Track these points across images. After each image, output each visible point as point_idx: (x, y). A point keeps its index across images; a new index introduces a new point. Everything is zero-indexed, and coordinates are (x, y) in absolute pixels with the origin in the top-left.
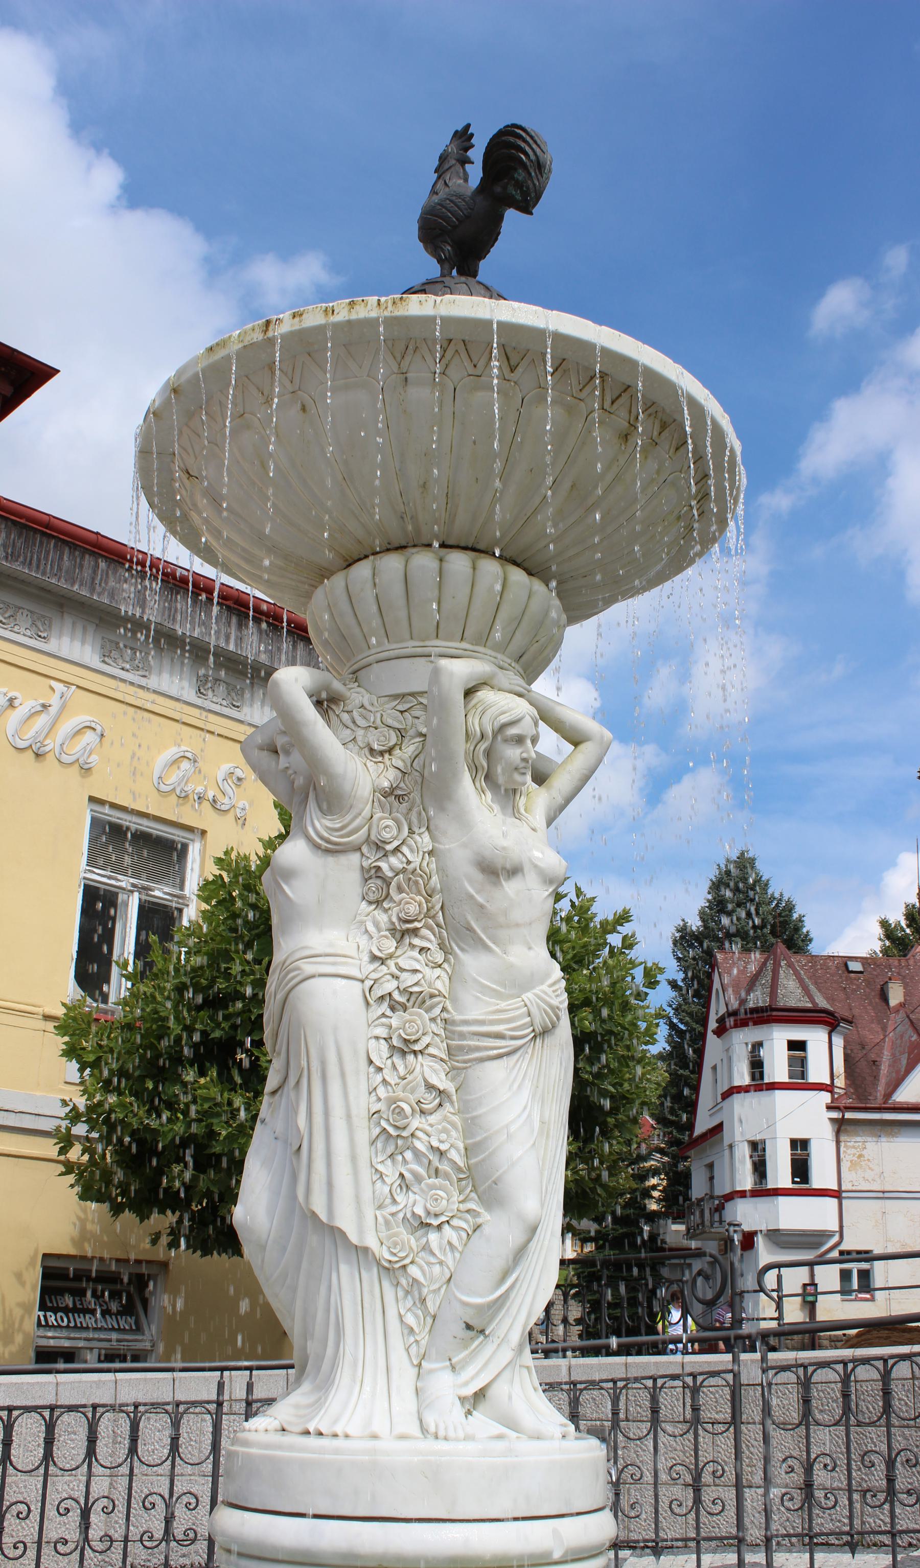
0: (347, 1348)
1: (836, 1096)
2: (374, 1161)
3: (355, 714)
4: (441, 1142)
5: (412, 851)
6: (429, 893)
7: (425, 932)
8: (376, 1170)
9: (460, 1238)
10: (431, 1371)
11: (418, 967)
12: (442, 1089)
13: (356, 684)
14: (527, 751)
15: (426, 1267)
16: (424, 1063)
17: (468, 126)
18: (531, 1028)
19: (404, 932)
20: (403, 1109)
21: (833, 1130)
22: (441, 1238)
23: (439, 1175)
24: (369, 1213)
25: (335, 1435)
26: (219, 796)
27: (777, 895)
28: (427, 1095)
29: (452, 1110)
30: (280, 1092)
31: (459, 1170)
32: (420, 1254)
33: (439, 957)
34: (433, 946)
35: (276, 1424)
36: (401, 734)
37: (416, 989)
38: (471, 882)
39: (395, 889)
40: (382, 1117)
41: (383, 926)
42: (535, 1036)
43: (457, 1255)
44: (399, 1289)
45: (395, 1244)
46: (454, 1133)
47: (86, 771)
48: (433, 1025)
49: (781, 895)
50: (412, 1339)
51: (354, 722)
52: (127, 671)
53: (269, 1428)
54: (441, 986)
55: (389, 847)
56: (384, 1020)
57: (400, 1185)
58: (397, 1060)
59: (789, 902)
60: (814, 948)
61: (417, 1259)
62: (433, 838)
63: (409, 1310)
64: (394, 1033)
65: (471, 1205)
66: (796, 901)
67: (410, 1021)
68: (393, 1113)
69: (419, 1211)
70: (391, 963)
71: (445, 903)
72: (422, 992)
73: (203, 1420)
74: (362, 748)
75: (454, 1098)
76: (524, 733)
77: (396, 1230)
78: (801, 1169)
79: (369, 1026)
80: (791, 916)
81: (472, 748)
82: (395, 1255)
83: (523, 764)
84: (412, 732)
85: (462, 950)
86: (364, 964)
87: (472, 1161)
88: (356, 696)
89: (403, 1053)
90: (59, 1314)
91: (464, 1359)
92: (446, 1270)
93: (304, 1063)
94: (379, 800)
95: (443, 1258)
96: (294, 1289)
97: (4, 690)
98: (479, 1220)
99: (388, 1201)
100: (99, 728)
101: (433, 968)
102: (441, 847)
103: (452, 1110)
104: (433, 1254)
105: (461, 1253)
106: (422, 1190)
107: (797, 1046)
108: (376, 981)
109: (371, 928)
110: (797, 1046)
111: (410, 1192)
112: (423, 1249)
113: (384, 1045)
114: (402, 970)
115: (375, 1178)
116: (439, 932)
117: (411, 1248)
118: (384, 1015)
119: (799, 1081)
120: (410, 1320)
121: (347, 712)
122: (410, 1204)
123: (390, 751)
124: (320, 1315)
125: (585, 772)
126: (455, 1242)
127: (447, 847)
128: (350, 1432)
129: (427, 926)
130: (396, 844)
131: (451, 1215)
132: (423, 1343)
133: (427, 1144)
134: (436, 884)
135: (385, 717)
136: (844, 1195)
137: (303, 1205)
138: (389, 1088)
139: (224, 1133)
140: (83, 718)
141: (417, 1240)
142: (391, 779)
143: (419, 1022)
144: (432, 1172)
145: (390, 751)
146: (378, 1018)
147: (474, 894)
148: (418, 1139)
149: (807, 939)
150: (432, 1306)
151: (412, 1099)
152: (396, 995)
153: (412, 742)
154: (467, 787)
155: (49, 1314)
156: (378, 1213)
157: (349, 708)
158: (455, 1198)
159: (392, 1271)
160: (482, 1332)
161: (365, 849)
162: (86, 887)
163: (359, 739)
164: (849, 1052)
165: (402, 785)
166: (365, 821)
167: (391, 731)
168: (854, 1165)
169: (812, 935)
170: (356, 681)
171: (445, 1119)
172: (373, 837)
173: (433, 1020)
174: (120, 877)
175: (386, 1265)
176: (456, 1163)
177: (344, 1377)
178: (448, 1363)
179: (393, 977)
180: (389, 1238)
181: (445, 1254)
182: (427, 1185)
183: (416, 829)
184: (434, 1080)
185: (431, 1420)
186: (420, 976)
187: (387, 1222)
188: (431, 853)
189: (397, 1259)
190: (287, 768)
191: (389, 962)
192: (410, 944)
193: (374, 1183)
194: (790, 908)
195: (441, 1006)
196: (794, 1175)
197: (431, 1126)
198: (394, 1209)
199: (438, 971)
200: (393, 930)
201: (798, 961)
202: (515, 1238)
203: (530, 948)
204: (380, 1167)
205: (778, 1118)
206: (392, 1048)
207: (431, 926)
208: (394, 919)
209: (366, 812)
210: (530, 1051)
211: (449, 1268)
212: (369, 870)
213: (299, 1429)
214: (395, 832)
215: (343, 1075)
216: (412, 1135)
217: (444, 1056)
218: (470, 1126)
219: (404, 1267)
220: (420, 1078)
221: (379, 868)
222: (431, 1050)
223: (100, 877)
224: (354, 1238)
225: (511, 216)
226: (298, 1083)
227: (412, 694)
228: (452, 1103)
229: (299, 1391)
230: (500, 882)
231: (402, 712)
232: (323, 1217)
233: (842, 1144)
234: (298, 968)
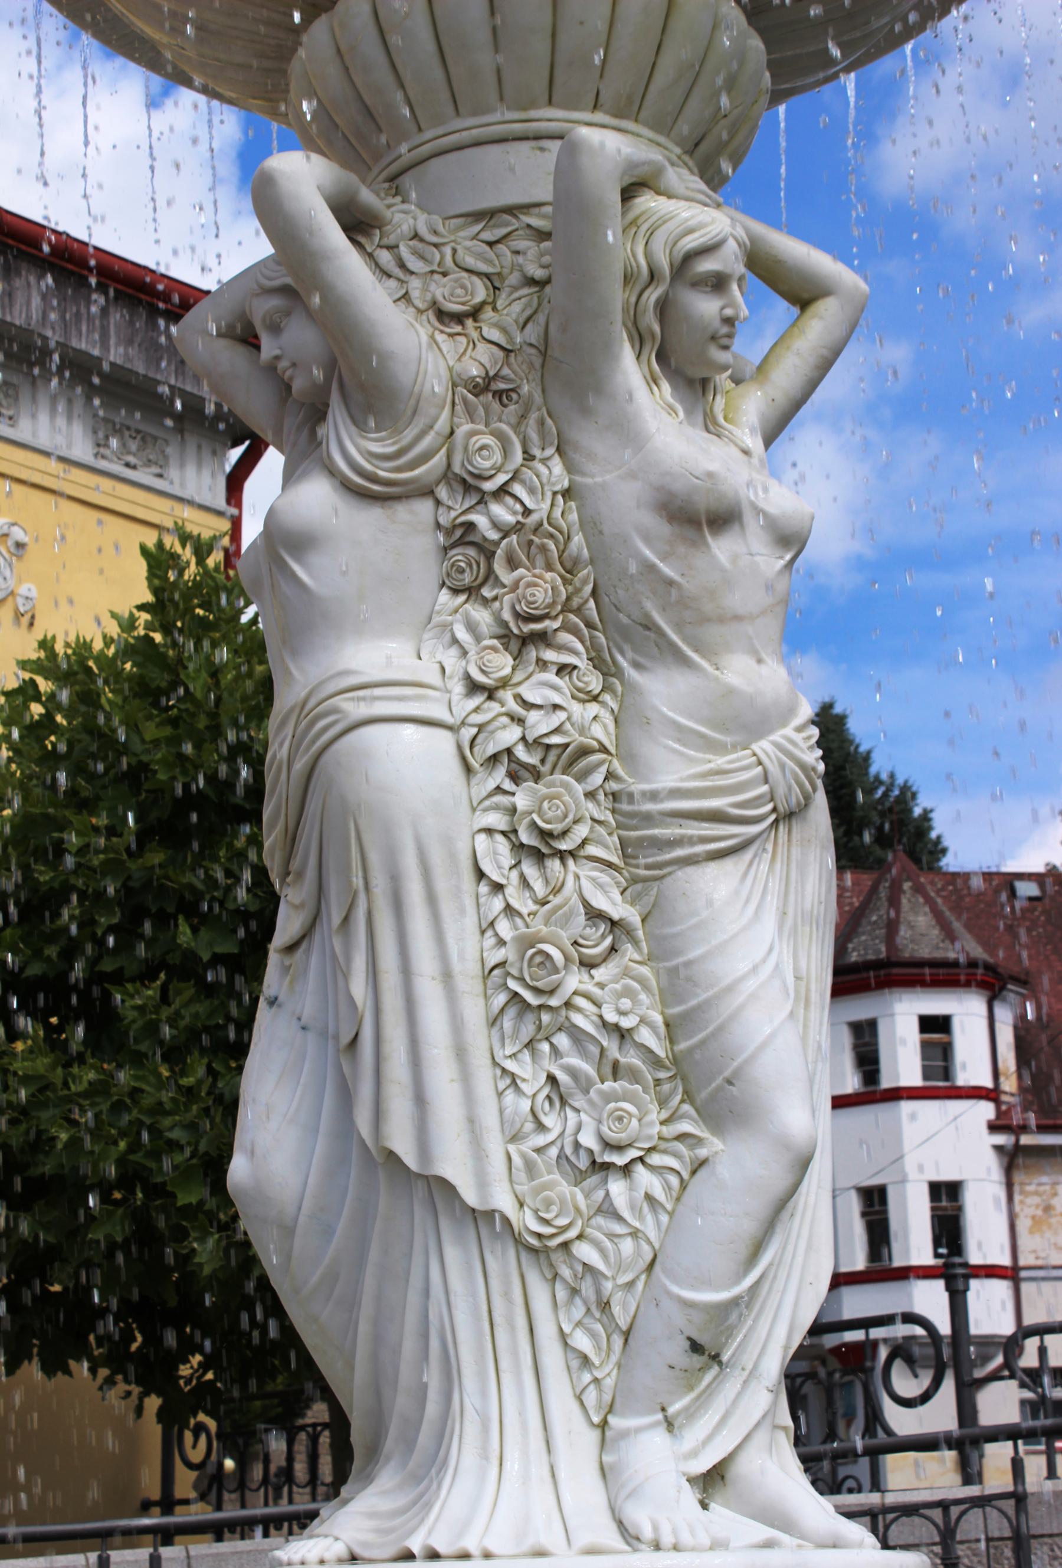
0: (466, 1400)
1: (1004, 1108)
2: (499, 1055)
3: (404, 251)
4: (622, 1013)
5: (532, 491)
6: (569, 565)
8: (504, 1070)
9: (668, 1187)
10: (625, 1434)
11: (553, 699)
12: (616, 917)
13: (399, 199)
14: (732, 304)
15: (608, 1244)
16: (581, 874)
18: (770, 806)
19: (524, 638)
20: (548, 956)
21: (1001, 1164)
22: (631, 1189)
23: (620, 1075)
24: (495, 1146)
25: (465, 1556)
27: (884, 776)
28: (588, 931)
29: (636, 957)
30: (304, 945)
31: (656, 1062)
32: (593, 1222)
33: (595, 682)
34: (582, 663)
35: (339, 1549)
36: (493, 281)
37: (555, 740)
38: (647, 540)
39: (503, 562)
40: (508, 974)
41: (484, 629)
42: (776, 821)
43: (664, 1218)
44: (559, 1286)
45: (548, 1204)
46: (643, 997)
48: (590, 805)
49: (892, 776)
50: (587, 1377)
51: (402, 265)
53: (327, 1556)
54: (602, 732)
55: (489, 486)
56: (499, 799)
57: (548, 1097)
58: (529, 869)
59: (905, 788)
60: (950, 863)
61: (589, 1230)
63: (579, 1324)
64: (520, 820)
65: (685, 1127)
66: (918, 783)
67: (551, 798)
68: (530, 966)
69: (588, 1140)
70: (507, 695)
71: (600, 582)
72: (567, 745)
74: (420, 312)
75: (640, 933)
76: (728, 271)
77: (547, 1178)
78: (948, 1229)
79: (474, 810)
80: (910, 811)
81: (633, 299)
82: (547, 1222)
83: (725, 330)
84: (514, 279)
85: (637, 665)
86: (455, 698)
87: (682, 1046)
88: (404, 218)
89: (539, 857)
91: (686, 1409)
92: (646, 1247)
93: (358, 882)
94: (465, 401)
95: (637, 1224)
96: (352, 1304)
98: (703, 1152)
99: (529, 1126)
101: (584, 701)
102: (588, 481)
103: (636, 957)
104: (620, 1218)
105: (671, 1214)
106: (591, 1102)
107: (935, 1026)
108: (481, 727)
109: (462, 634)
110: (935, 1026)
111: (568, 1110)
112: (599, 1211)
113: (502, 845)
114: (528, 706)
115: (502, 1085)
116: (592, 637)
117: (578, 1210)
118: (499, 790)
119: (940, 1083)
120: (582, 1341)
121: (389, 248)
122: (570, 1130)
123: (475, 313)
124: (409, 1346)
125: (825, 352)
126: (659, 1193)
127: (598, 479)
128: (493, 1548)
129: (566, 627)
130: (502, 478)
131: (647, 1146)
132: (609, 1383)
133: (595, 1019)
134: (580, 549)
135: (460, 252)
136: (1023, 1274)
138: (518, 921)
139: (64, 1136)
141: (587, 1196)
142: (485, 360)
143: (567, 798)
144: (608, 1070)
145: (475, 313)
146: (490, 795)
147: (657, 562)
148: (579, 1010)
149: (938, 850)
150: (622, 1316)
151: (565, 936)
152: (521, 752)
153: (516, 295)
154: (630, 369)
156: (512, 1148)
157: (391, 240)
158: (654, 1115)
159: (543, 1252)
160: (716, 1358)
163: (415, 294)
164: (1023, 1033)
165: (506, 371)
166: (441, 440)
167: (475, 279)
168: (1037, 1224)
169: (946, 842)
170: (396, 194)
171: (626, 973)
172: (457, 469)
173: (590, 795)
175: (533, 1241)
176: (651, 1051)
177: (466, 1453)
178: (660, 1416)
179: (512, 719)
180: (537, 1191)
181: (641, 1218)
182: (601, 1093)
183: (537, 452)
184: (600, 902)
185: (641, 1518)
186: (562, 716)
187: (530, 1167)
188: (567, 494)
189: (553, 1231)
190: (277, 358)
191: (501, 694)
192: (539, 660)
193: (500, 1094)
194: (907, 796)
195: (603, 770)
196: (937, 1243)
197: (601, 986)
198: (541, 1140)
199: (593, 708)
200: (505, 637)
201: (932, 883)
202: (774, 1176)
203: (760, 661)
204: (510, 1065)
205: (907, 1146)
206: (519, 848)
207: (576, 625)
208: (507, 615)
209: (442, 423)
210: (770, 847)
211: (649, 1243)
212: (449, 532)
213: (392, 1551)
214: (497, 457)
215: (432, 899)
216: (568, 1004)
217: (615, 859)
218: (676, 982)
219: (565, 1245)
220: (575, 899)
221: (470, 526)
222: (592, 850)
224: (470, 1197)
226: (346, 920)
227: (511, 210)
228: (635, 942)
229: (372, 1489)
230: (703, 537)
231: (491, 244)
232: (411, 1161)
233: (1016, 1188)
234: (335, 710)
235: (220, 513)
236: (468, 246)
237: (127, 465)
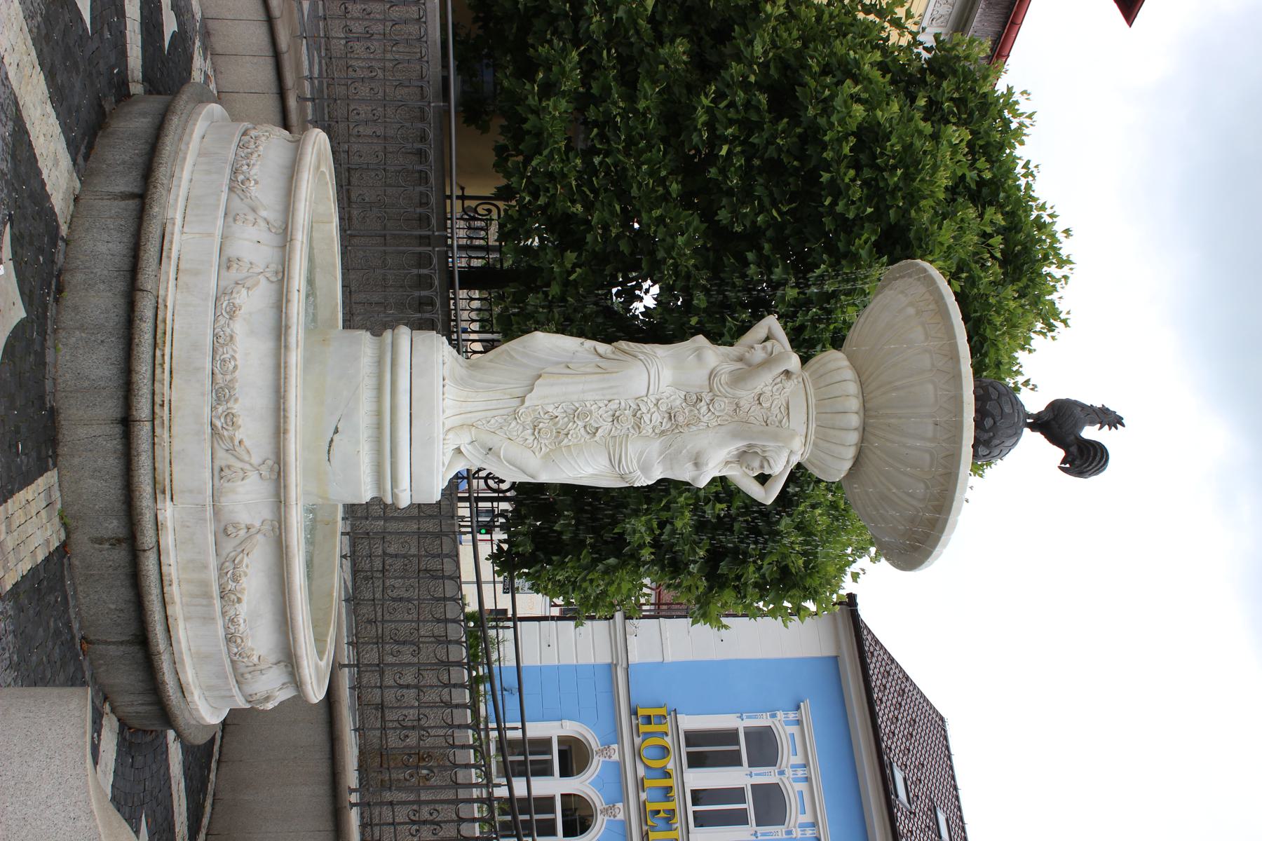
17: (1123, 425)
113: (616, 406)
159: (515, 415)
225: (1060, 453)
236: (780, 401)
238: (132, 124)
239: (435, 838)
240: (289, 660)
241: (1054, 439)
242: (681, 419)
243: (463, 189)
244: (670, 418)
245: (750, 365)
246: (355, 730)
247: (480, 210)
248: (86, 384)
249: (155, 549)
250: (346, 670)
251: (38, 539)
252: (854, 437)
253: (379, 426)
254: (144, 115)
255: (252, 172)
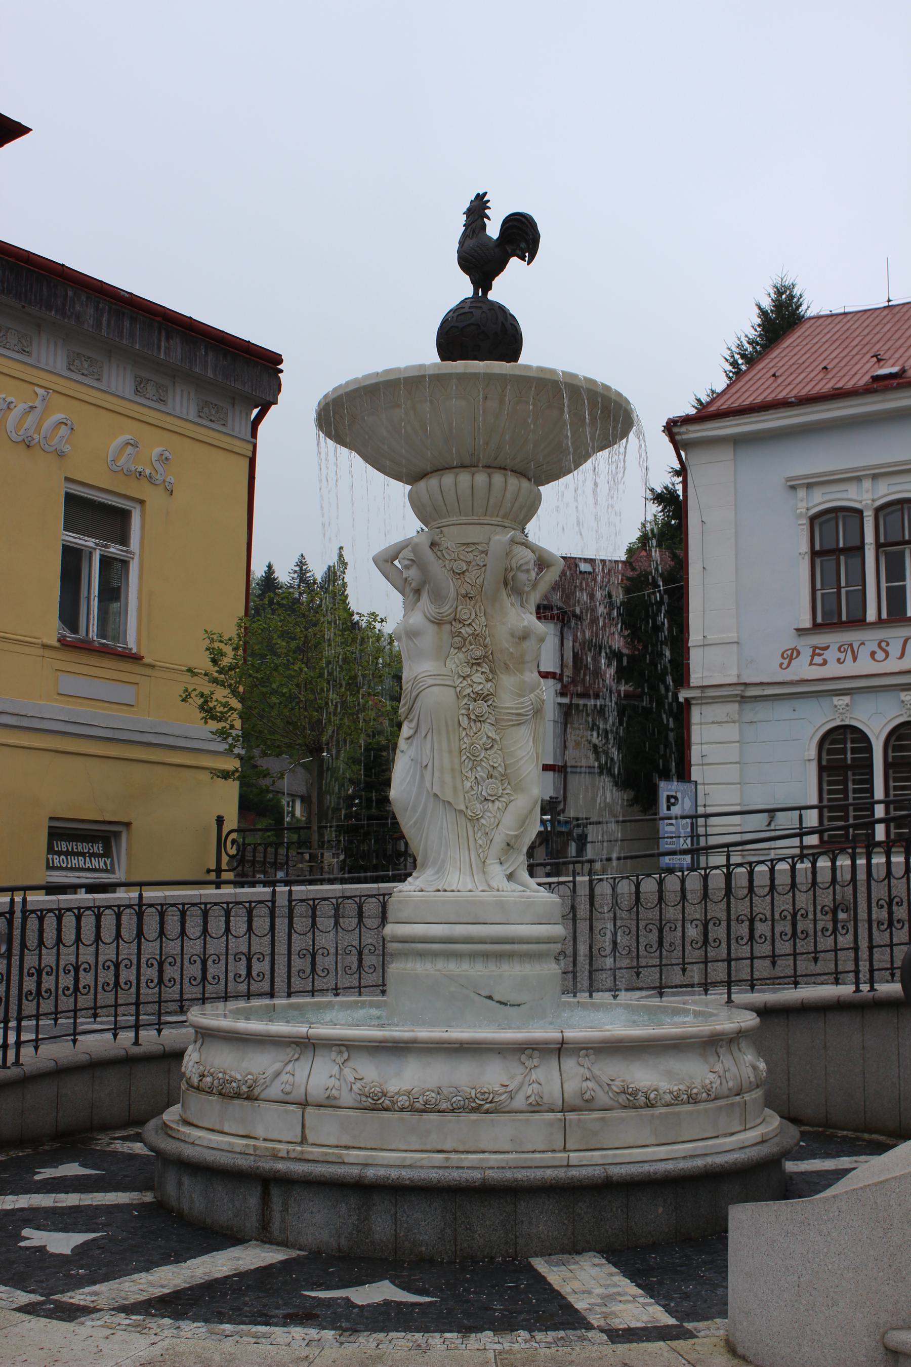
7: (484, 664)
17: (485, 194)
19: (476, 663)
26: (154, 473)
34: (488, 672)
47: (61, 455)
52: (86, 375)
55: (466, 623)
58: (472, 724)
62: (486, 619)
69: (484, 793)
73: (220, 921)
84: (474, 563)
90: (62, 857)
97: (4, 396)
100: (69, 423)
113: (466, 718)
136: (569, 770)
137: (429, 789)
140: (59, 416)
145: (463, 573)
152: (472, 695)
155: (55, 857)
159: (474, 820)
161: (453, 623)
162: (64, 546)
174: (87, 538)
184: (490, 735)
187: (469, 799)
206: (469, 718)
223: (74, 539)
225: (514, 262)
235: (248, 442)
237: (211, 420)
238: (191, 1197)
239: (905, 904)
240: (712, 1044)
241: (500, 267)
242: (479, 653)
243: (209, 871)
244: (479, 664)
245: (424, 583)
246: (796, 988)
247: (233, 852)
248: (448, 1231)
249: (607, 1167)
250: (733, 996)
251: (595, 1271)
252: (498, 478)
253: (486, 956)
254: (180, 1184)
255: (239, 1077)
